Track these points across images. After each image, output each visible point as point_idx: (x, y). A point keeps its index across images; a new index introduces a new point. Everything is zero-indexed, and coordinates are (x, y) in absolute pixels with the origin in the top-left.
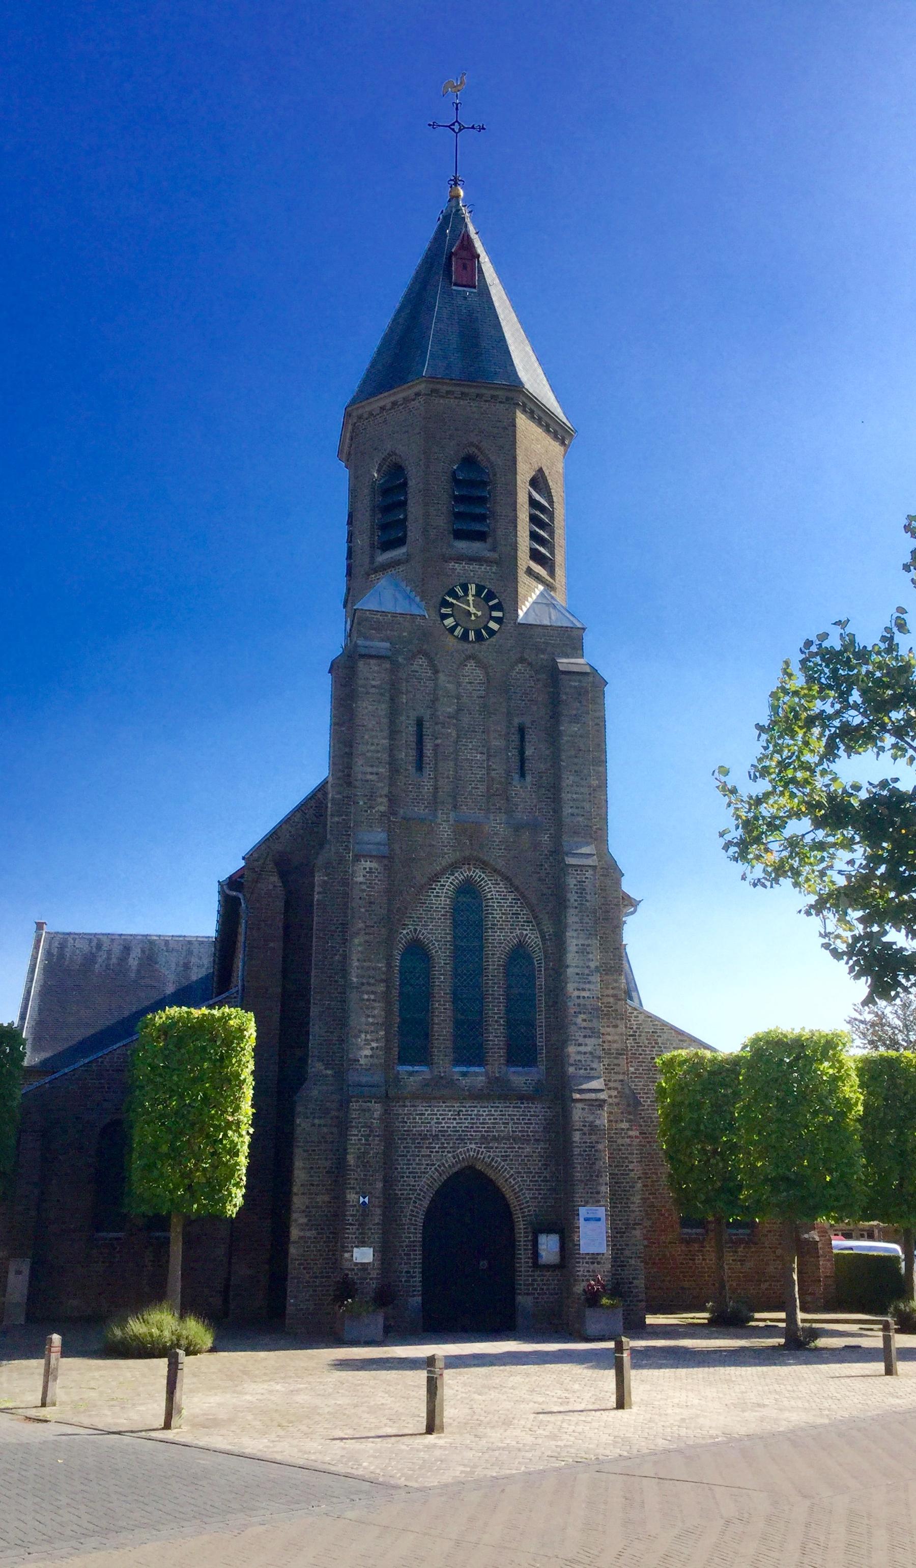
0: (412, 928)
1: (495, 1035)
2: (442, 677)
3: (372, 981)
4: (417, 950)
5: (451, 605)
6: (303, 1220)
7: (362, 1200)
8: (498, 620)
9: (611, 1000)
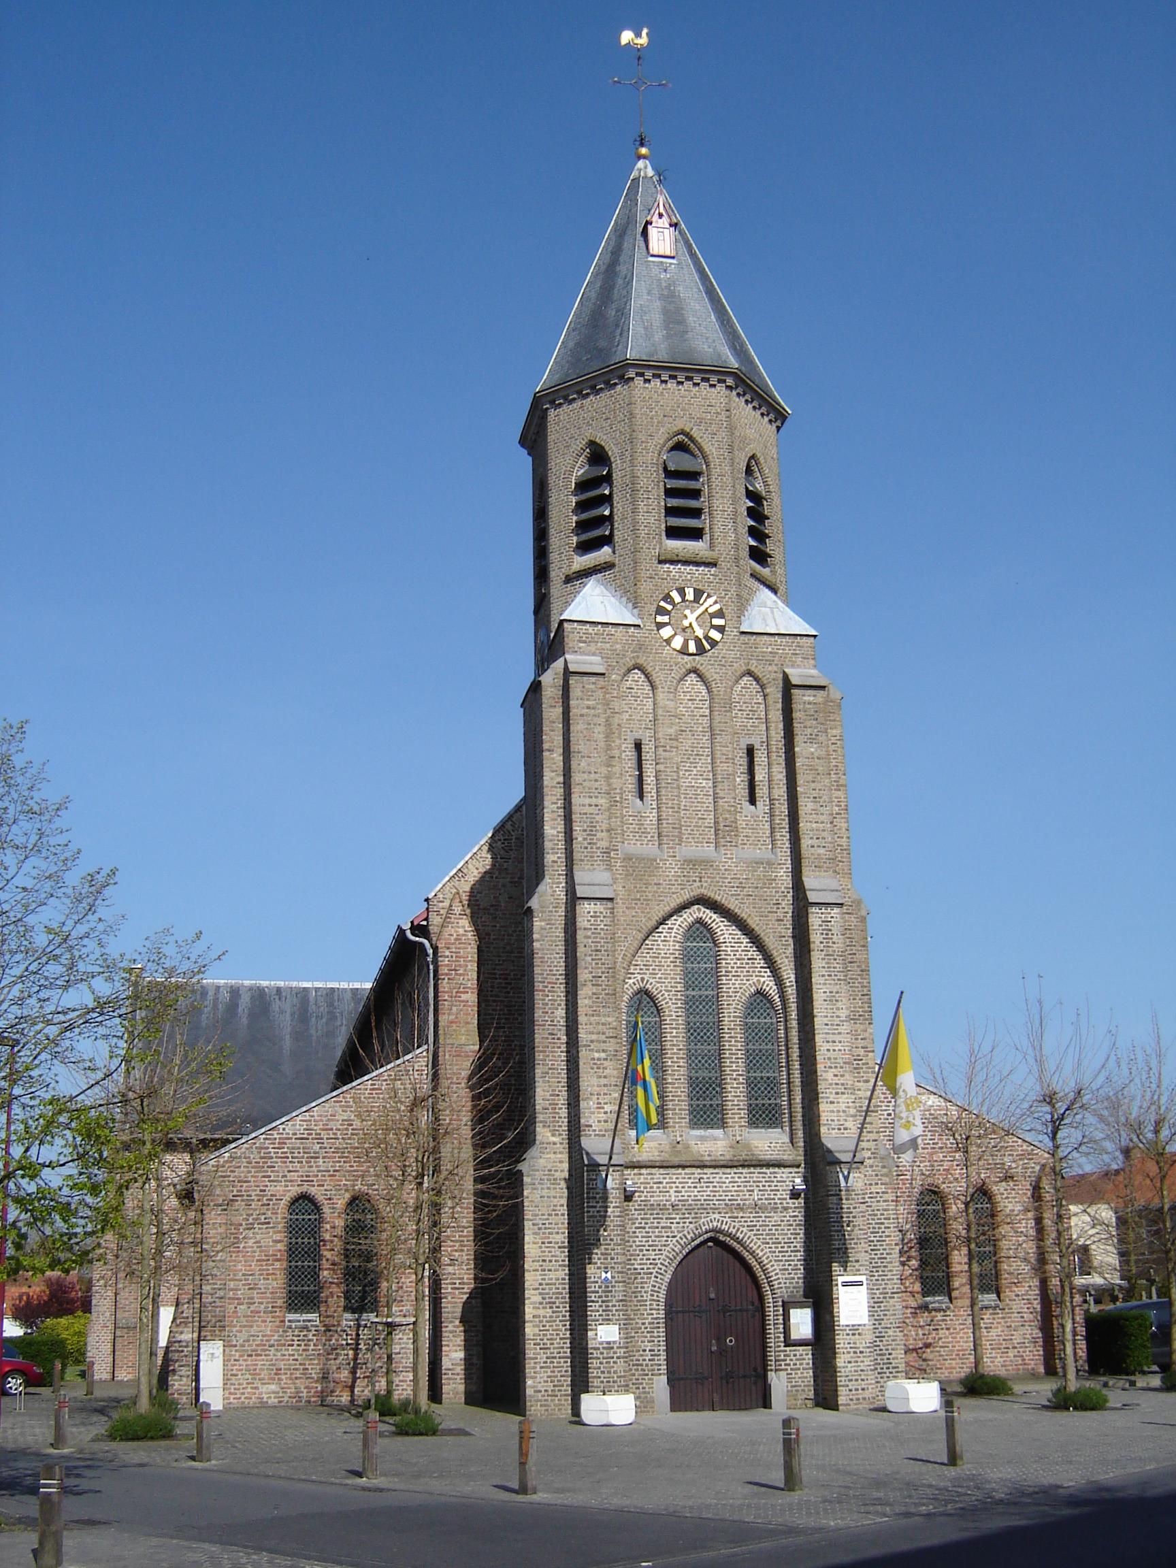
0: (639, 977)
1: (736, 1094)
2: (661, 696)
3: (603, 1037)
4: (645, 999)
5: (667, 613)
6: (538, 1299)
7: (604, 1275)
8: (721, 629)
9: (862, 1052)
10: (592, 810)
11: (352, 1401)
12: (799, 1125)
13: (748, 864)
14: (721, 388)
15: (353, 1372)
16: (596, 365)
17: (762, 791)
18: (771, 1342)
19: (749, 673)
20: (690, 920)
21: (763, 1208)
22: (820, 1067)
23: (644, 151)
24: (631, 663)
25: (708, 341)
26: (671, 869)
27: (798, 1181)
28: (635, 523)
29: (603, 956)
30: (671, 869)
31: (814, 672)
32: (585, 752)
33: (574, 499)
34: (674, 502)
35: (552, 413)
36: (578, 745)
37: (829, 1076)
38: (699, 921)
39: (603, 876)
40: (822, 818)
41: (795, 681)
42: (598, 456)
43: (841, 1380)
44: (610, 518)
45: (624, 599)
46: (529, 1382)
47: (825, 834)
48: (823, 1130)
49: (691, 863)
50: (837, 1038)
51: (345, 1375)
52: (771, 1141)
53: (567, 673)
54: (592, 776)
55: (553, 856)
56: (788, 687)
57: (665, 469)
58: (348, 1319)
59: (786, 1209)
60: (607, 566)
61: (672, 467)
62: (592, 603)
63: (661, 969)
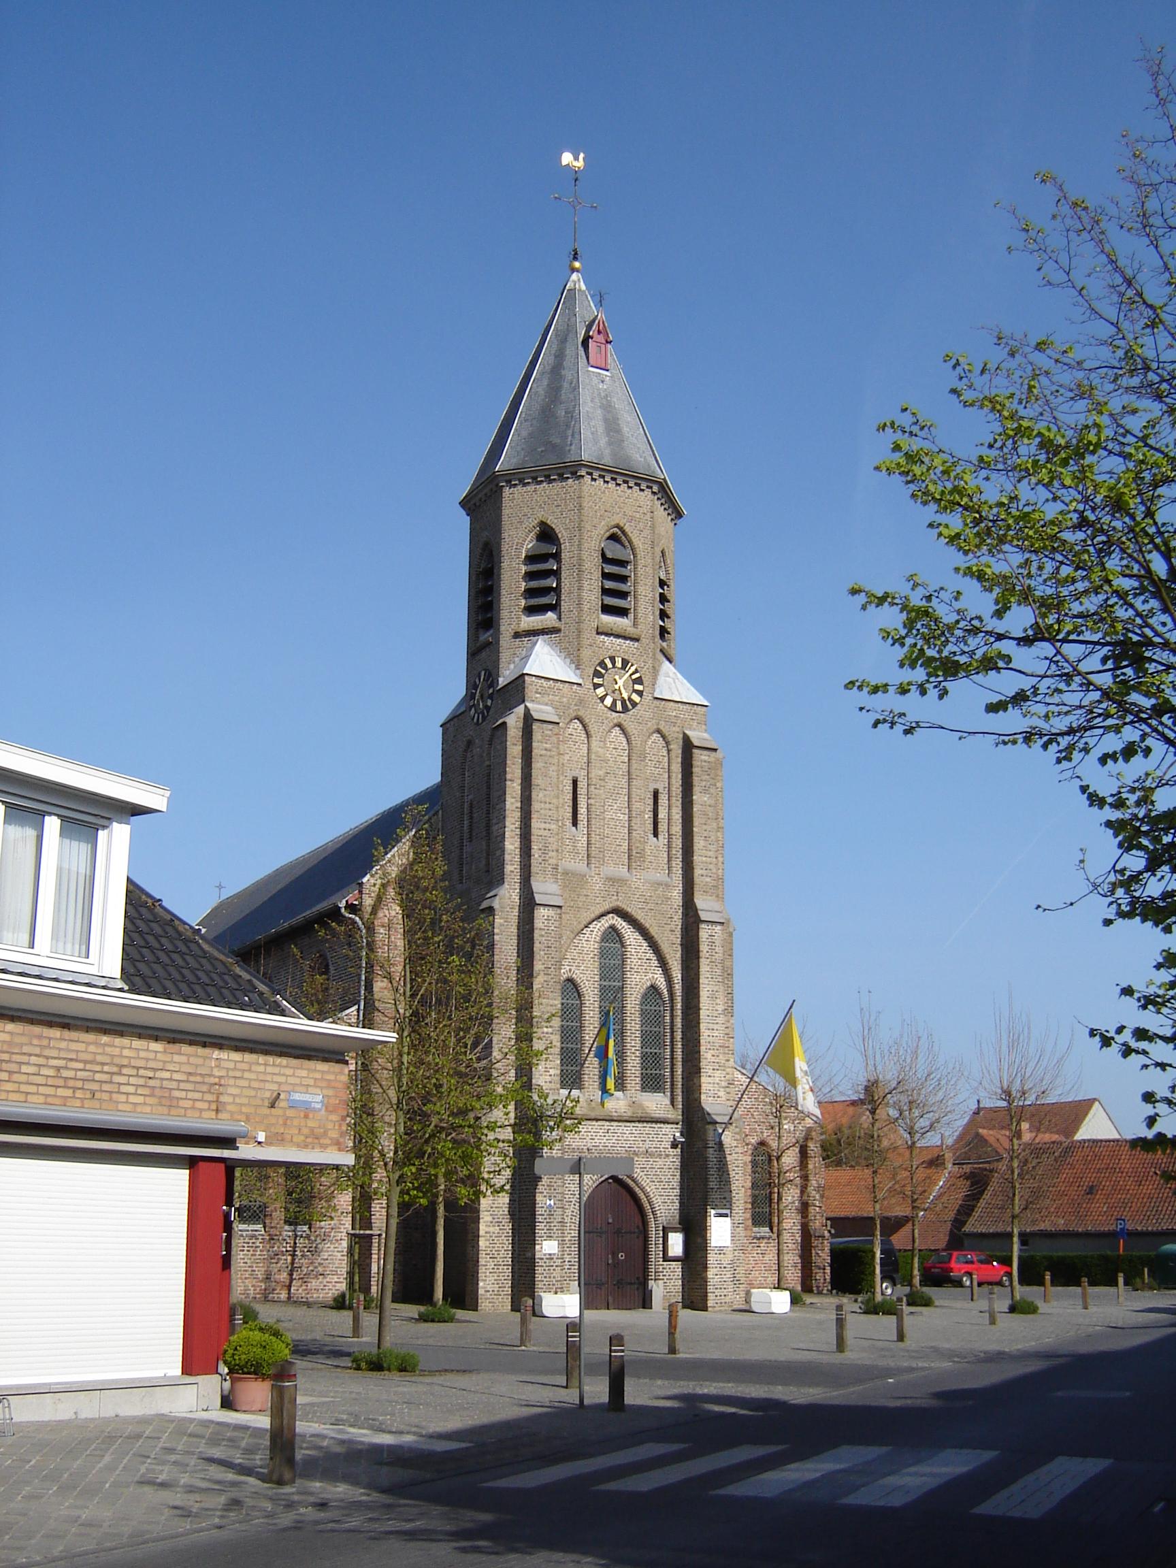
2: (594, 744)
6: (490, 1219)
8: (640, 693)
10: (546, 833)
11: (289, 1298)
12: (679, 1091)
13: (653, 889)
14: (648, 492)
15: (291, 1275)
16: (552, 459)
17: (663, 827)
18: (652, 1258)
19: (659, 731)
20: (607, 925)
21: (652, 1155)
22: (703, 1049)
23: (577, 264)
24: (574, 714)
25: (640, 454)
26: (596, 884)
27: (678, 1134)
28: (580, 598)
29: (552, 951)
30: (596, 884)
31: (706, 735)
32: (543, 786)
33: (524, 569)
34: (609, 584)
35: (507, 491)
36: (537, 779)
37: (709, 1056)
38: (613, 927)
39: (553, 887)
40: (710, 854)
41: (696, 743)
42: (546, 534)
43: (710, 1289)
44: (557, 591)
45: (568, 660)
46: (481, 1284)
47: (711, 866)
48: (703, 1097)
49: (612, 880)
50: (715, 1027)
51: (284, 1276)
52: (657, 1103)
53: (528, 720)
54: (547, 806)
55: (512, 867)
56: (688, 746)
57: (603, 555)
58: (287, 1231)
59: (667, 1156)
60: (555, 631)
61: (609, 555)
62: (544, 661)
63: (583, 964)
